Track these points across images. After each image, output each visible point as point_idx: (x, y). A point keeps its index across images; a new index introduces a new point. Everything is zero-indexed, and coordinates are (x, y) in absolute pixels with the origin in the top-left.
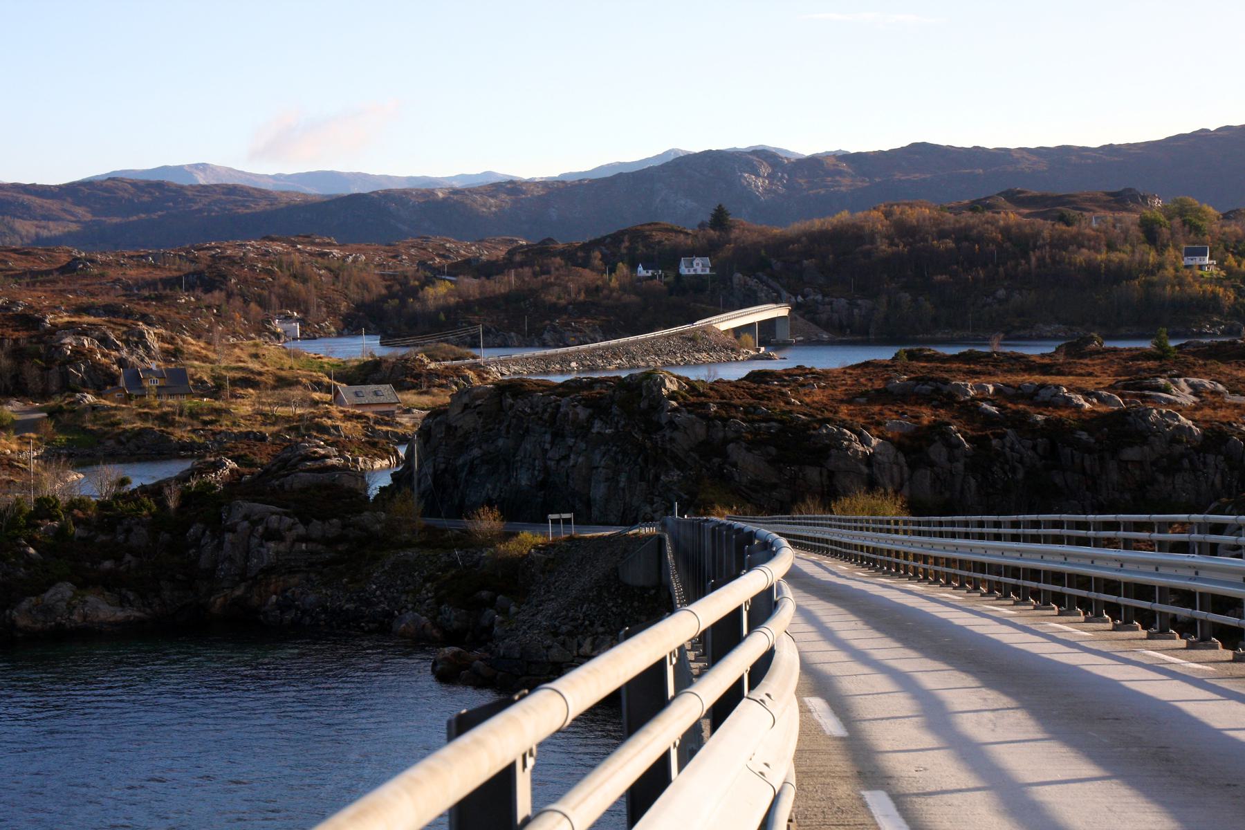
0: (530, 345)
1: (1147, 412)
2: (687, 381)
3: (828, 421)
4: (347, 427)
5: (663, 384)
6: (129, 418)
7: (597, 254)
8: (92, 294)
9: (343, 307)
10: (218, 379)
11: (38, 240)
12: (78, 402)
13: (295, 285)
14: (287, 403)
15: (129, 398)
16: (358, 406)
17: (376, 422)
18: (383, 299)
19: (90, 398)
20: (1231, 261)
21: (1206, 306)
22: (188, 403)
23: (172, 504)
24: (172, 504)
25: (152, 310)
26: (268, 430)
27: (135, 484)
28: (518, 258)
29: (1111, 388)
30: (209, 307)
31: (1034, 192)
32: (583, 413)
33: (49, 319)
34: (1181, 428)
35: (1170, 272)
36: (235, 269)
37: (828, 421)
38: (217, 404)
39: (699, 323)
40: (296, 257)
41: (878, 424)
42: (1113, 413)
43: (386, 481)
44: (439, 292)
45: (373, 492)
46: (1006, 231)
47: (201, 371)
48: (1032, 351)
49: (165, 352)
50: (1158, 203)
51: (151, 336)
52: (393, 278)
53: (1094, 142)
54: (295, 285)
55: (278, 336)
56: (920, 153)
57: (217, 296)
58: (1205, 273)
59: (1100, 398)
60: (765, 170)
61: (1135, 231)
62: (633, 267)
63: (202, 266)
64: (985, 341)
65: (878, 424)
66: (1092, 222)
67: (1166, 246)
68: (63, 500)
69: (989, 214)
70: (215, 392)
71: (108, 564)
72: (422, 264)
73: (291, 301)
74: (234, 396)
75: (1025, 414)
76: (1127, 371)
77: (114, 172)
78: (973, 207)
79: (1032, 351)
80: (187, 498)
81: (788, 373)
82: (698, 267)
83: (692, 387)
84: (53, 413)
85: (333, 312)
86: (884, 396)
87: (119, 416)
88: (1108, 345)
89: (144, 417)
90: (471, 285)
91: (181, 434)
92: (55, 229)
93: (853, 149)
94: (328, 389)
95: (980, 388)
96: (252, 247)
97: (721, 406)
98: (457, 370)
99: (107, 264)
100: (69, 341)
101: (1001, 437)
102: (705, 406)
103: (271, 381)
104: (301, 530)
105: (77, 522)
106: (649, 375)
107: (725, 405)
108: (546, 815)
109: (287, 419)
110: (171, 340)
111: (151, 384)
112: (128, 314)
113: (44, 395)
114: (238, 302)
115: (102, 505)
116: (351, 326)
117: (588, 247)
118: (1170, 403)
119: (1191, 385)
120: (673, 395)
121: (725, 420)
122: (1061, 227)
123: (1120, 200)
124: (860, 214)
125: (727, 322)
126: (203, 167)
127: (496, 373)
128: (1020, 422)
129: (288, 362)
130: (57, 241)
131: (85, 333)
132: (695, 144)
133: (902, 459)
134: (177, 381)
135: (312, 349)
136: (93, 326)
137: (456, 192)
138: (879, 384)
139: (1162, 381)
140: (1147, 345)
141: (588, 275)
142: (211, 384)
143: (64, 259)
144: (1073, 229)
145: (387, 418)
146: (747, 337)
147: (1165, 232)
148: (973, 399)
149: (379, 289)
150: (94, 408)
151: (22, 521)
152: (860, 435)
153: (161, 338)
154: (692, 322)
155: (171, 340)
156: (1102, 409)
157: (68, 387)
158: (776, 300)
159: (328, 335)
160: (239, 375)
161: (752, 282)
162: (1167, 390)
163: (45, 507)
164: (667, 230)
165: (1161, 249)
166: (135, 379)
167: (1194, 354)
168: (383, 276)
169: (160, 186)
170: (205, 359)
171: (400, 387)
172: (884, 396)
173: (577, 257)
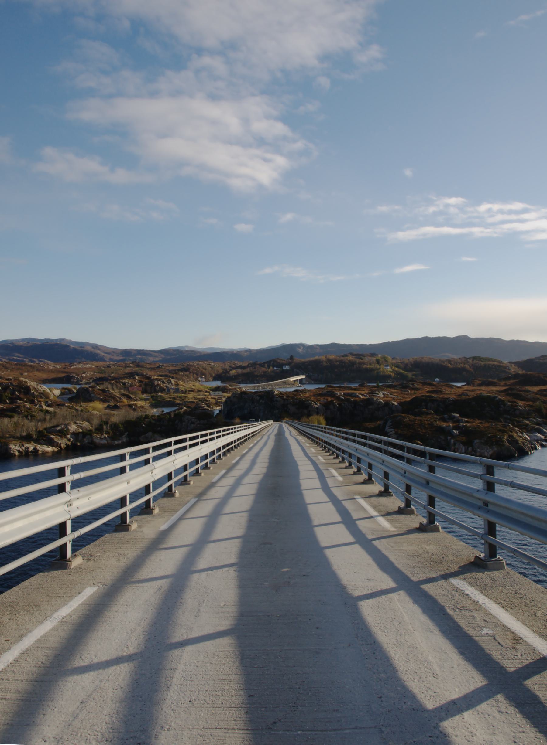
0: (252, 383)
1: (374, 398)
2: (280, 391)
3: (309, 400)
4: (212, 400)
5: (275, 392)
6: (167, 398)
7: (266, 365)
8: (163, 372)
9: (214, 375)
10: (186, 390)
11: (154, 361)
12: (157, 395)
13: (204, 371)
14: (199, 395)
15: (167, 394)
16: (214, 396)
17: (218, 399)
18: (221, 374)
19: (160, 394)
20: (393, 368)
21: (389, 377)
22: (179, 395)
23: (172, 416)
24: (172, 416)
25: (174, 376)
26: (195, 401)
27: (165, 412)
28: (250, 365)
29: (367, 393)
30: (186, 375)
31: (356, 353)
32: (258, 398)
33: (153, 378)
34: (380, 402)
35: (382, 370)
36: (192, 367)
37: (309, 400)
38: (185, 395)
39: (286, 379)
40: (204, 365)
41: (319, 401)
42: (366, 399)
43: (218, 412)
44: (233, 372)
45: (215, 414)
46: (349, 361)
47: (182, 388)
48: (353, 386)
49: (175, 384)
50: (380, 356)
51: (173, 381)
52: (224, 369)
53: (368, 344)
54: (204, 371)
55: (200, 381)
56: (333, 345)
57: (188, 373)
58: (389, 370)
59: (364, 396)
60: (302, 348)
61: (375, 361)
62: (274, 368)
63: (185, 367)
64: (343, 383)
65: (319, 401)
66: (366, 359)
67: (381, 364)
68: (150, 415)
69: (346, 357)
70: (185, 393)
71: (159, 428)
72: (230, 366)
73: (203, 374)
74: (189, 394)
75: (349, 399)
76: (371, 390)
77: (179, 347)
78: (343, 356)
79: (353, 386)
80: (176, 415)
81: (302, 390)
82: (287, 367)
83: (281, 393)
84: (152, 397)
85: (211, 376)
86: (320, 395)
87: (165, 397)
88: (368, 384)
89: (170, 398)
90: (240, 371)
91: (178, 401)
92: (157, 359)
93: (320, 344)
94: (208, 392)
95: (341, 393)
96: (195, 363)
97: (286, 397)
98: (235, 389)
99: (166, 366)
100: (156, 382)
101: (344, 403)
102: (283, 397)
103: (196, 390)
104: (198, 422)
105: (153, 420)
106: (272, 390)
107: (288, 397)
108: (201, 501)
109: (199, 399)
110: (177, 382)
111: (172, 391)
112: (170, 377)
113: (151, 393)
114: (192, 374)
115: (158, 416)
116: (216, 378)
117: (264, 363)
118: (378, 396)
119: (383, 393)
120: (277, 395)
121: (287, 400)
122: (360, 360)
123: (372, 355)
124: (320, 357)
125: (292, 379)
126: (187, 346)
127: (244, 389)
128: (348, 400)
129: (201, 387)
130: (157, 361)
131: (159, 380)
132: (288, 342)
133: (324, 408)
134: (177, 391)
135: (206, 384)
136: (161, 379)
137: (238, 352)
138: (321, 392)
139: (377, 392)
140: (375, 384)
141: (264, 369)
142: (184, 391)
143: (158, 365)
144: (363, 361)
145: (220, 398)
146: (296, 382)
147: (381, 362)
148: (339, 396)
149: (221, 371)
150: (160, 396)
151: (142, 419)
152: (316, 403)
153: (175, 381)
154: (285, 379)
155: (177, 382)
156: (365, 398)
157: (156, 391)
158: (303, 374)
159: (210, 381)
160: (190, 389)
161: (298, 371)
162: (378, 394)
163: (147, 417)
164: (280, 360)
165: (380, 365)
166: (169, 390)
167: (385, 387)
168: (222, 369)
169: (178, 350)
170: (183, 386)
171: (223, 392)
172: (320, 395)
173: (262, 365)
